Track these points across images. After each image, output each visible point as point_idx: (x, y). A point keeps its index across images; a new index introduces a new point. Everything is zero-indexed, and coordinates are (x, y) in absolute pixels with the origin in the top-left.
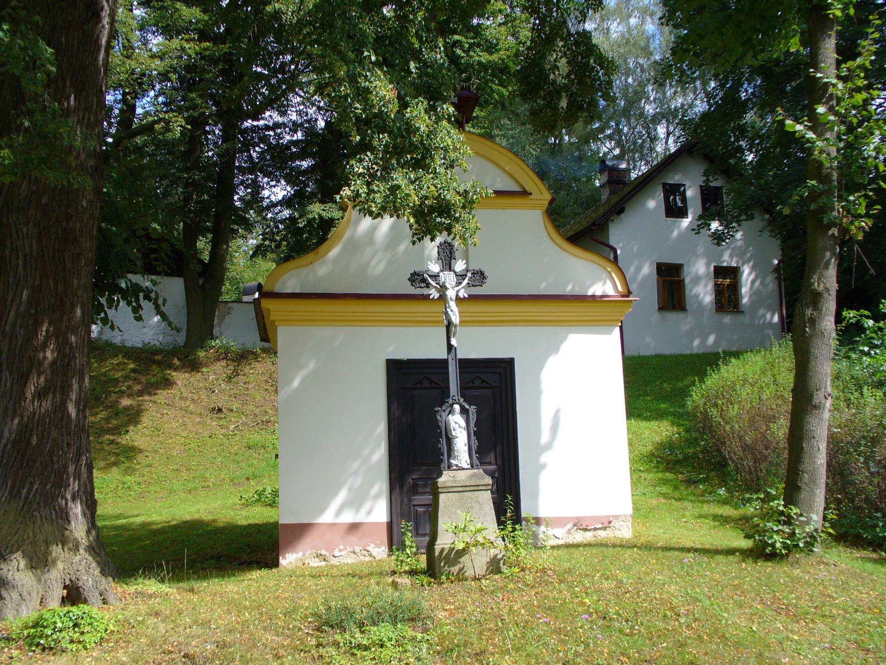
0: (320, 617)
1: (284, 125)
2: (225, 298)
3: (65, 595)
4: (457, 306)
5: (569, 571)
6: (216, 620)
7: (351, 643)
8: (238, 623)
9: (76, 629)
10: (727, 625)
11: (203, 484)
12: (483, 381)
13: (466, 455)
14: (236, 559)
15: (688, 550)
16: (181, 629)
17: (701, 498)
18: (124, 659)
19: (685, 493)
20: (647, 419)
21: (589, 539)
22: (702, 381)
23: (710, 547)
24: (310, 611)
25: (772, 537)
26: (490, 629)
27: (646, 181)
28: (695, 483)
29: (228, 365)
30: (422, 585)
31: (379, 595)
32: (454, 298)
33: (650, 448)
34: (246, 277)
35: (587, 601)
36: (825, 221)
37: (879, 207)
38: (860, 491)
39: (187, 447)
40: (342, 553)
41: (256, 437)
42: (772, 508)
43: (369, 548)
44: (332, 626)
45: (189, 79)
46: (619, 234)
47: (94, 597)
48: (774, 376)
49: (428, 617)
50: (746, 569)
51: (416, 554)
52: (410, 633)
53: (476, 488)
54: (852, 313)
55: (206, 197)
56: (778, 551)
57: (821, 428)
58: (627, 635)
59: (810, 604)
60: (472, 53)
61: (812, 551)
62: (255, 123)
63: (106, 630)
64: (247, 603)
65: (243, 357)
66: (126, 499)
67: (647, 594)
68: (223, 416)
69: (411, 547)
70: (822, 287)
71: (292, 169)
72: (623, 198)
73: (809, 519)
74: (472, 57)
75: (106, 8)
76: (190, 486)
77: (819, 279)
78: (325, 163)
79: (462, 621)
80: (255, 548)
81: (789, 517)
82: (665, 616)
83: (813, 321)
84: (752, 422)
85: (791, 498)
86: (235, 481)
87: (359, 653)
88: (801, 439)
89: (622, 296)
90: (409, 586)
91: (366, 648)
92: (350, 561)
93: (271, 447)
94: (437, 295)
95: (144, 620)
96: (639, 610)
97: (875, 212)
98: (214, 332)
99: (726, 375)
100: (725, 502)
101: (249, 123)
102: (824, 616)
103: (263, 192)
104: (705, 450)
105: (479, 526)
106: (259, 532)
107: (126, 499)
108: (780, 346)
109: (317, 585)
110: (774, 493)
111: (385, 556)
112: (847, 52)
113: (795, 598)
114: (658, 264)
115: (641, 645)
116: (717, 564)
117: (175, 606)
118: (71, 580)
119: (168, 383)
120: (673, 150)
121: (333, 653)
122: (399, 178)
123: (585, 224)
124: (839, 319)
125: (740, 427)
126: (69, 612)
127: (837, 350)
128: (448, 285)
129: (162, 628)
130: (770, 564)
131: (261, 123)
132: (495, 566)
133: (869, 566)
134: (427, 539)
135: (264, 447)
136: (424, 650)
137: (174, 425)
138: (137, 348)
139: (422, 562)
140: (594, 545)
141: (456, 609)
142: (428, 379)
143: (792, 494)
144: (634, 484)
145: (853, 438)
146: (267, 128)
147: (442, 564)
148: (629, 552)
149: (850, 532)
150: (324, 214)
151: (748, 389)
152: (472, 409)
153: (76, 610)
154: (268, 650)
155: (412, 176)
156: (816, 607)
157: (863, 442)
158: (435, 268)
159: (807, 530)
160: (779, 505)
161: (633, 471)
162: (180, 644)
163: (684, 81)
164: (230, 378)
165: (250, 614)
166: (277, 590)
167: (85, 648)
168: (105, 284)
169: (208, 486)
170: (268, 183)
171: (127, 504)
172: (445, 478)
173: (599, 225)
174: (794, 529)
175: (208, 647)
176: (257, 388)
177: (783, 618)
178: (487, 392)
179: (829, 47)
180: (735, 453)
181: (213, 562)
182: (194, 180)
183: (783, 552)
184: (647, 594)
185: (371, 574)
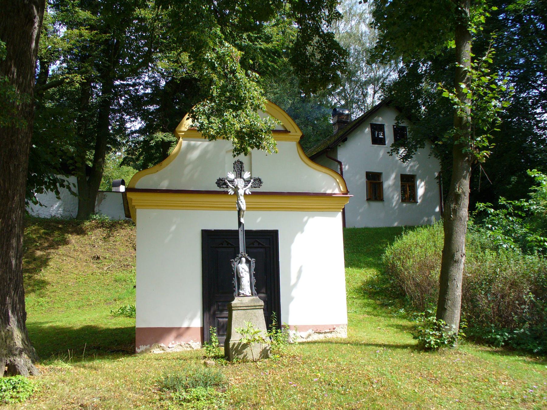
0: (162, 383)
2: (101, 188)
3: (6, 370)
4: (245, 198)
5: (309, 357)
7: (180, 398)
9: (15, 390)
10: (401, 389)
12: (259, 243)
13: (249, 288)
14: (109, 349)
15: (380, 346)
16: (78, 390)
18: (44, 407)
19: (380, 311)
20: (360, 267)
22: (391, 244)
24: (156, 379)
25: (429, 338)
26: (261, 391)
27: (361, 122)
28: (387, 305)
32: (243, 194)
33: (360, 284)
34: (115, 175)
35: (319, 374)
36: (463, 151)
37: (494, 144)
38: (483, 310)
39: (78, 280)
41: (121, 275)
44: (169, 389)
45: (81, 56)
46: (343, 154)
48: (435, 242)
51: (218, 346)
52: (215, 392)
53: (254, 308)
54: (482, 205)
58: (342, 394)
59: (449, 377)
60: (256, 43)
61: (452, 346)
63: (33, 391)
64: (118, 375)
65: (112, 226)
67: (354, 371)
68: (100, 261)
69: (215, 342)
70: (461, 190)
73: (451, 327)
74: (256, 45)
75: (38, 17)
76: (80, 304)
80: (120, 343)
81: (439, 326)
83: (455, 211)
84: (420, 269)
85: (441, 314)
86: (108, 301)
87: (184, 404)
89: (343, 194)
90: (214, 365)
91: (189, 401)
92: (178, 350)
93: (130, 281)
96: (349, 380)
97: (492, 147)
98: (95, 209)
99: (406, 241)
100: (404, 317)
101: (117, 83)
104: (392, 286)
105: (256, 330)
108: (439, 224)
109: (159, 365)
110: (431, 312)
111: (200, 347)
112: (478, 50)
113: (441, 374)
115: (350, 400)
118: (10, 361)
119: (66, 242)
120: (377, 103)
121: (169, 404)
123: (323, 147)
124: (472, 208)
126: (10, 380)
127: (472, 226)
128: (239, 187)
129: (67, 389)
130: (427, 354)
131: (125, 82)
132: (265, 354)
133: (485, 355)
134: (225, 337)
135: (125, 281)
136: (223, 402)
137: (70, 266)
138: (47, 219)
141: (242, 379)
142: (227, 242)
143: (441, 314)
144: (349, 306)
145: (479, 280)
148: (345, 346)
150: (165, 138)
151: (419, 249)
152: (253, 261)
153: (14, 379)
154: (130, 402)
158: (232, 176)
159: (449, 334)
161: (348, 299)
162: (78, 398)
163: (384, 61)
165: (119, 381)
167: (20, 401)
168: (35, 183)
169: (91, 305)
170: (130, 119)
171: (40, 315)
172: (236, 302)
173: (332, 148)
175: (95, 400)
177: (433, 385)
178: (262, 250)
179: (468, 47)
182: (84, 116)
183: (435, 347)
184: (354, 371)
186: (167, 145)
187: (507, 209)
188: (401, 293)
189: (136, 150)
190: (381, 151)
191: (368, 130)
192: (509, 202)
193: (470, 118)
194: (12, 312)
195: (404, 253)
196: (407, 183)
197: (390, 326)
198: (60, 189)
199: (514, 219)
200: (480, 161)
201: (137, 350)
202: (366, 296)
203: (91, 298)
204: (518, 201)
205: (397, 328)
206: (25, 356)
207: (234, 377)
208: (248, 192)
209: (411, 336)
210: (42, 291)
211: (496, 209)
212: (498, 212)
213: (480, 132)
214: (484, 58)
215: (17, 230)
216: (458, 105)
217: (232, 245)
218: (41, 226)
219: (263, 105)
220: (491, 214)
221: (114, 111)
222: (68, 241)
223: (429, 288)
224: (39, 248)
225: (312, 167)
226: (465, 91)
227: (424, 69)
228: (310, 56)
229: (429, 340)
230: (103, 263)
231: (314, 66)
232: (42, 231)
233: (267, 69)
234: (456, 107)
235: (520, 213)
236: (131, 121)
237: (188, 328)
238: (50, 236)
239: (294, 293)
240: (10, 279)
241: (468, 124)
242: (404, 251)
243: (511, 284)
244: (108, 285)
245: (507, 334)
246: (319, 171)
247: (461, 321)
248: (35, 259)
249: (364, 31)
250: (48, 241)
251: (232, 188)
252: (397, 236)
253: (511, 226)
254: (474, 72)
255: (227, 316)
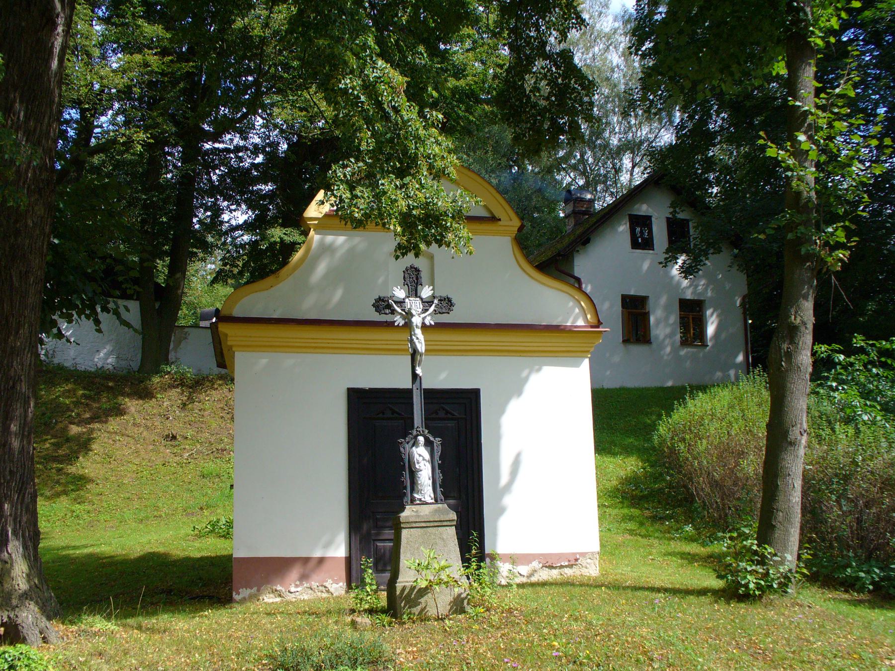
1: (245, 148)
5: (536, 612)
6: (164, 661)
8: (187, 665)
11: (156, 513)
12: (447, 412)
13: (430, 489)
14: (187, 593)
15: (658, 590)
17: (667, 535)
19: (651, 529)
20: (614, 454)
21: (555, 577)
23: (681, 587)
24: (265, 652)
25: (745, 578)
28: (662, 519)
29: (183, 391)
30: (384, 626)
31: (338, 637)
32: (420, 325)
33: (615, 483)
34: (204, 302)
35: (556, 643)
36: (803, 251)
37: (857, 239)
39: (139, 475)
40: (299, 589)
42: (745, 546)
43: (326, 584)
45: (145, 98)
46: (582, 265)
47: (33, 635)
49: (391, 660)
50: (719, 610)
51: (376, 591)
53: (440, 524)
55: (164, 220)
56: (751, 592)
57: (797, 464)
59: (787, 649)
61: (786, 592)
62: (217, 145)
64: (198, 643)
65: (195, 385)
66: (74, 528)
67: (618, 637)
68: (177, 443)
69: (371, 585)
70: (798, 321)
71: (252, 192)
72: (588, 229)
77: (796, 312)
78: (297, 173)
79: (425, 665)
80: (205, 583)
81: (763, 556)
82: (637, 661)
83: (789, 355)
84: (720, 457)
88: (776, 476)
89: (592, 327)
90: (369, 627)
92: (306, 597)
93: (226, 476)
94: (402, 323)
95: (86, 661)
96: (610, 654)
97: (853, 244)
100: (691, 539)
101: (207, 146)
102: (803, 662)
103: (223, 216)
105: (443, 563)
106: (212, 564)
107: (74, 528)
110: (747, 532)
111: (343, 592)
114: (622, 296)
116: (690, 605)
117: (121, 645)
118: (9, 617)
119: (119, 411)
122: (387, 184)
123: (549, 254)
125: (708, 463)
128: (413, 312)
130: (743, 605)
131: (221, 146)
132: (458, 606)
133: (844, 608)
135: (218, 476)
138: (90, 372)
139: (383, 600)
140: (561, 584)
141: (419, 651)
143: (766, 534)
144: (601, 518)
146: (228, 150)
147: (402, 605)
148: (597, 591)
149: (824, 574)
150: (286, 238)
152: (437, 441)
155: (398, 183)
156: (793, 653)
157: (835, 480)
159: (782, 570)
160: (752, 544)
164: (184, 405)
165: (200, 655)
166: (231, 628)
169: (161, 516)
170: (228, 207)
172: (408, 513)
174: (768, 570)
176: (212, 415)
178: (451, 424)
180: (702, 489)
181: (164, 596)
183: (757, 593)
184: (618, 637)
185: (329, 612)
186: (289, 249)
187: (868, 354)
188: (685, 499)
189: (238, 258)
190: (646, 261)
191: (623, 228)
192: (871, 342)
193: (813, 193)
194: (15, 533)
195: (690, 429)
196: (691, 313)
197: (670, 554)
198: (102, 316)
199: (881, 371)
200: (832, 269)
201: (236, 597)
202: (626, 503)
203: (160, 505)
204: (887, 340)
205: (682, 558)
206: (33, 607)
207: (404, 648)
208: (428, 321)
209: (713, 575)
210: (82, 493)
211: (848, 355)
212: (852, 359)
213: (833, 219)
214: (837, 90)
215: (23, 387)
216: (792, 171)
217: (400, 414)
218: (79, 384)
219: (451, 169)
220: (840, 363)
221: (203, 193)
222: (124, 409)
223: (736, 489)
224: (76, 421)
225: (536, 280)
226: (805, 146)
227: (720, 122)
228: (531, 91)
229: (746, 581)
230: (182, 447)
231: (539, 110)
232: (81, 392)
233: (458, 123)
234: (789, 174)
235: (889, 361)
236: (231, 211)
237: (321, 560)
238: (94, 401)
239: (507, 500)
240: (11, 471)
241: (810, 205)
242: (690, 426)
243: (882, 483)
244: (190, 483)
245: (877, 571)
246: (549, 286)
247: (800, 548)
248: (68, 440)
249: (615, 64)
250: (90, 410)
251: (400, 314)
252: (679, 402)
253: (875, 383)
254: (820, 113)
255: (392, 537)
